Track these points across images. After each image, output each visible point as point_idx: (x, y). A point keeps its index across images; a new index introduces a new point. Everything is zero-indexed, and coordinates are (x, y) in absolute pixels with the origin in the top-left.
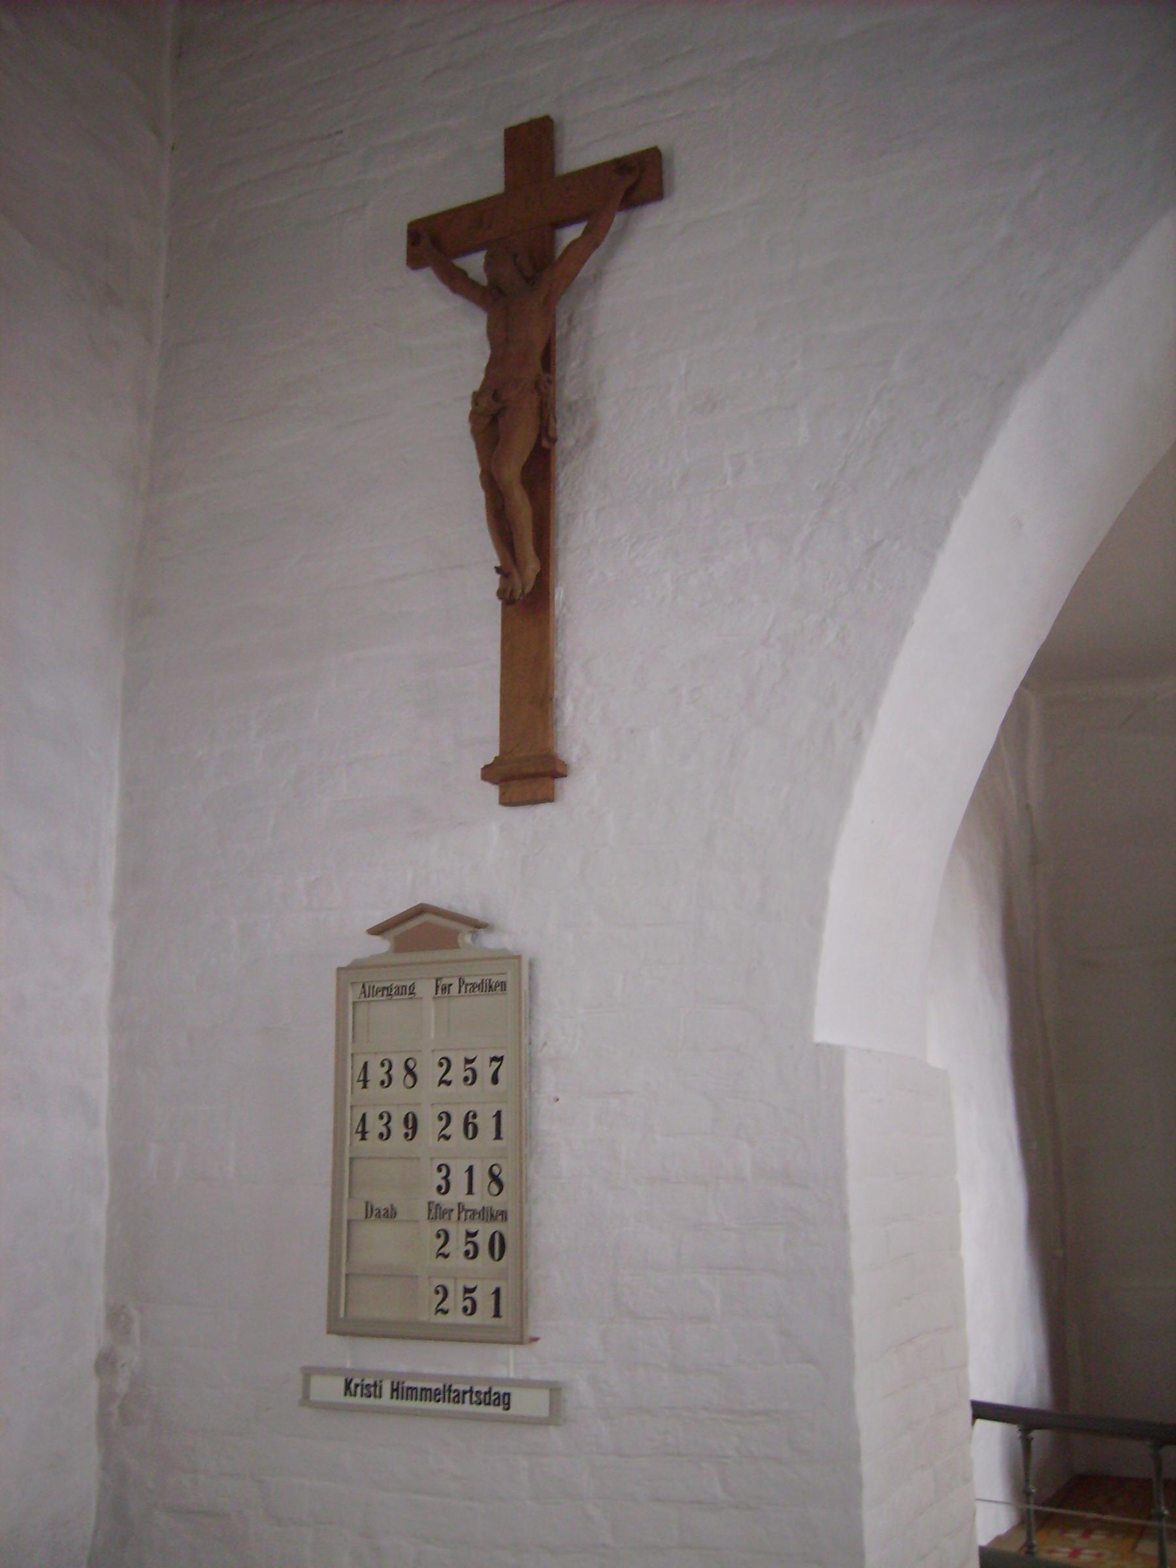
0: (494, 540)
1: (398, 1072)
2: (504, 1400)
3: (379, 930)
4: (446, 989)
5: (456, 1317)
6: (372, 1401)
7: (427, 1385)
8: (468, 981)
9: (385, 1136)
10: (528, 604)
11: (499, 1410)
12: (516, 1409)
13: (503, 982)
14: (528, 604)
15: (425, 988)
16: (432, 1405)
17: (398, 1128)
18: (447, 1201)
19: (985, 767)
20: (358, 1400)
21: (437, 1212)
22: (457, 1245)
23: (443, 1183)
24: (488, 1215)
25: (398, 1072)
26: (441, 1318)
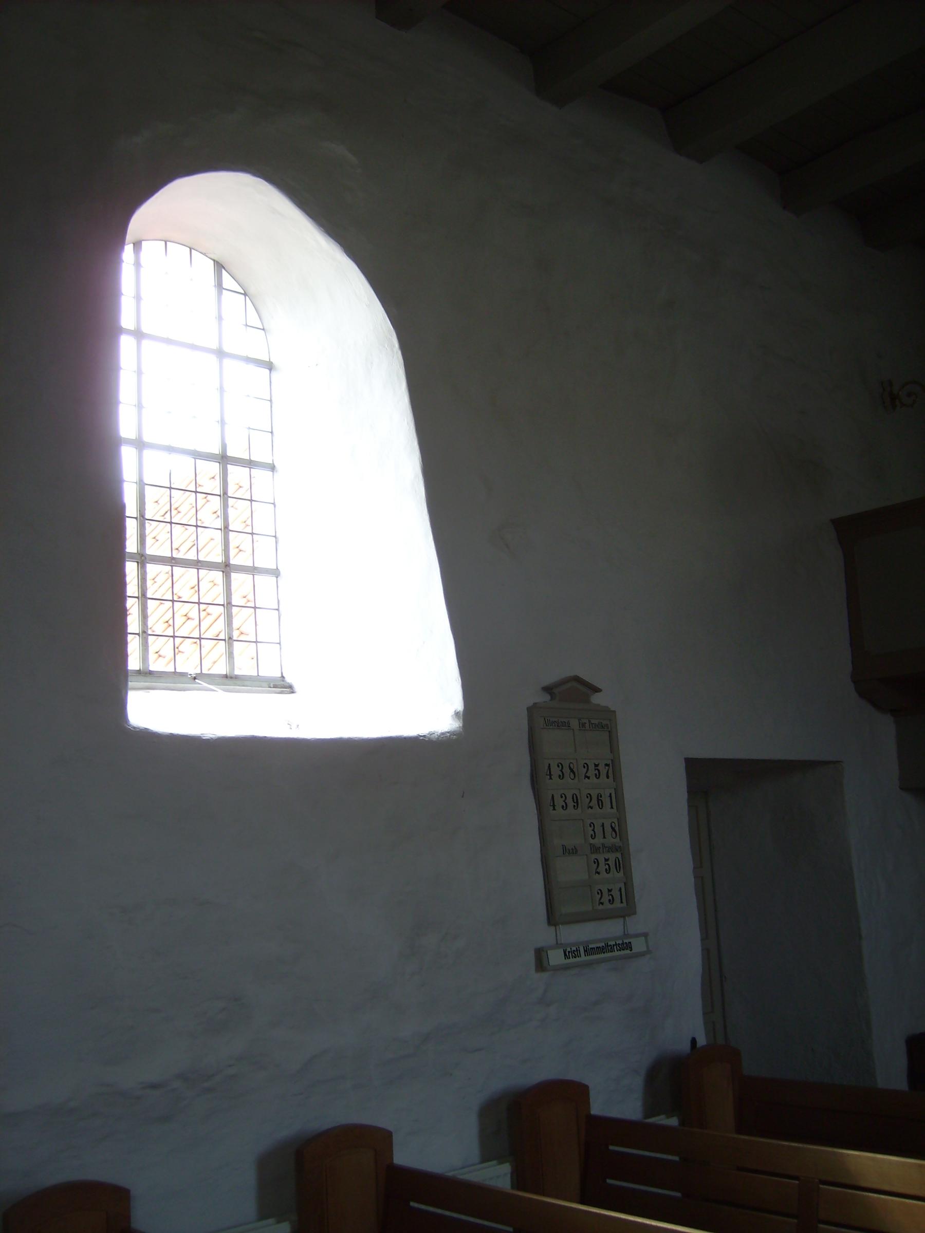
0: (266, 183)
1: (567, 771)
2: (629, 946)
3: (548, 689)
4: (584, 725)
5: (608, 906)
6: (578, 959)
7: (598, 945)
8: (593, 721)
9: (565, 807)
10: (248, 360)
11: (628, 952)
12: (636, 949)
13: (605, 724)
14: (248, 360)
15: (574, 723)
16: (602, 956)
17: (571, 804)
18: (598, 841)
19: (779, 761)
20: (572, 960)
21: (595, 849)
22: (602, 867)
23: (592, 832)
24: (613, 849)
25: (567, 771)
26: (601, 907)
